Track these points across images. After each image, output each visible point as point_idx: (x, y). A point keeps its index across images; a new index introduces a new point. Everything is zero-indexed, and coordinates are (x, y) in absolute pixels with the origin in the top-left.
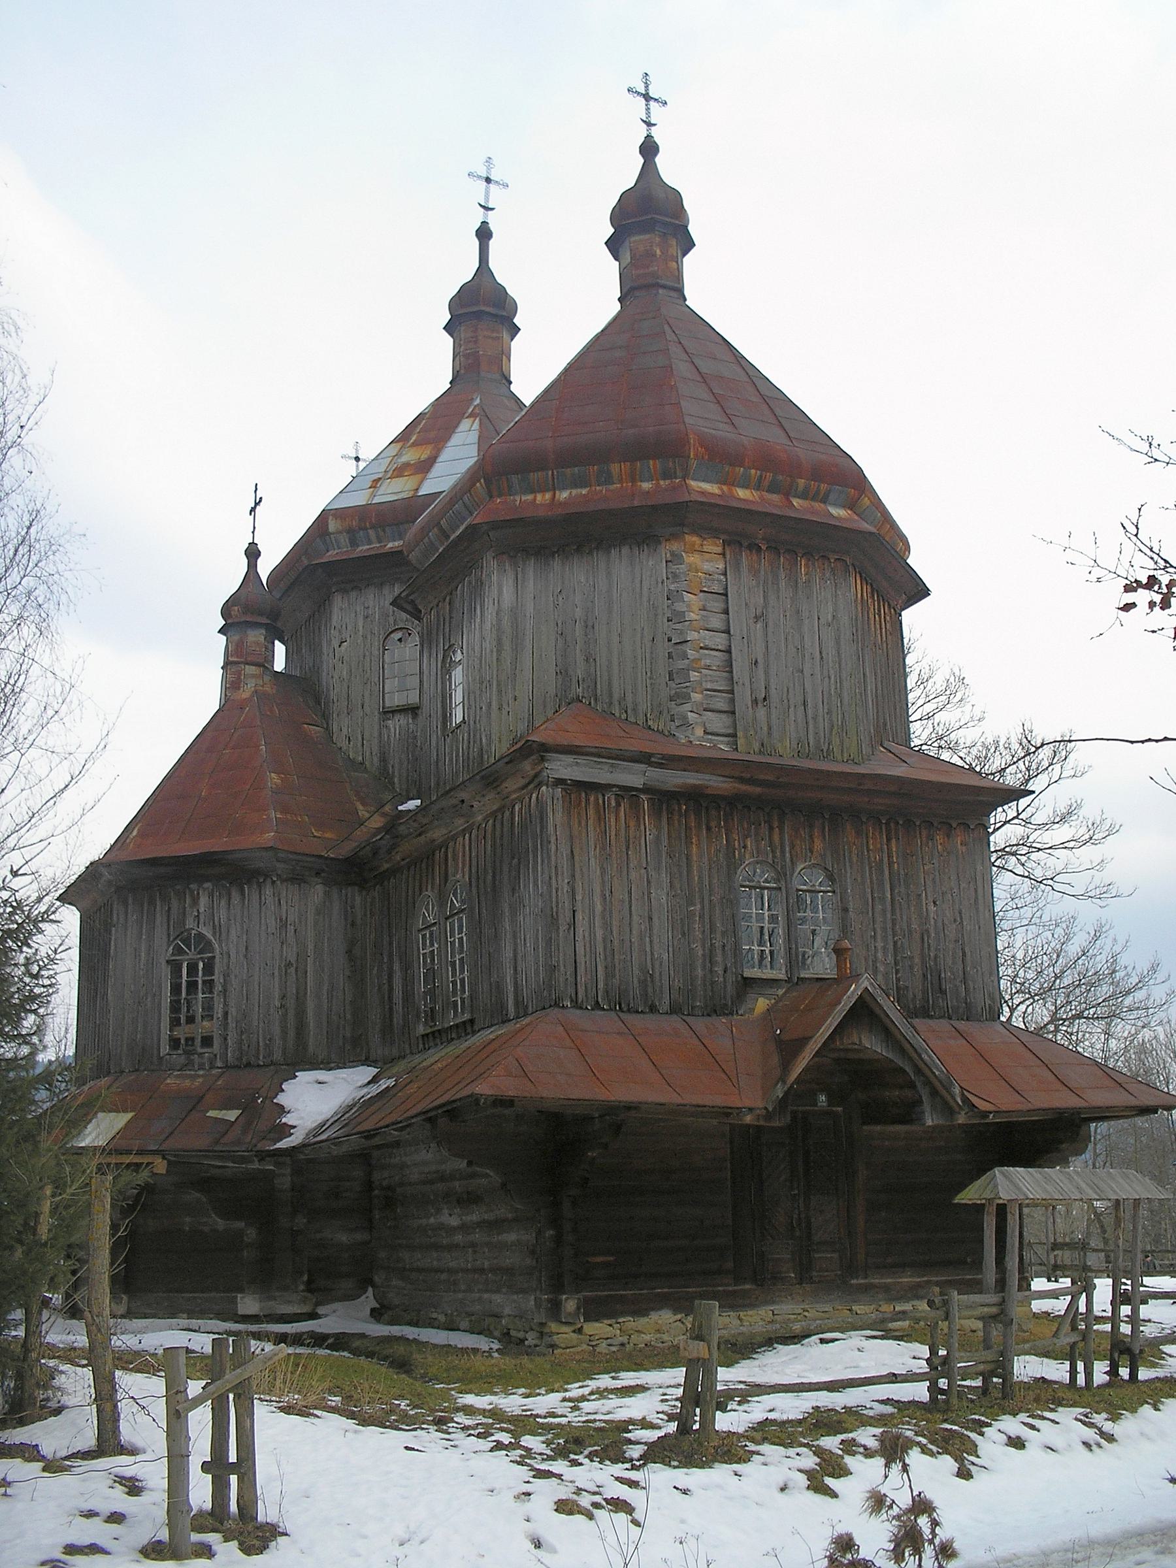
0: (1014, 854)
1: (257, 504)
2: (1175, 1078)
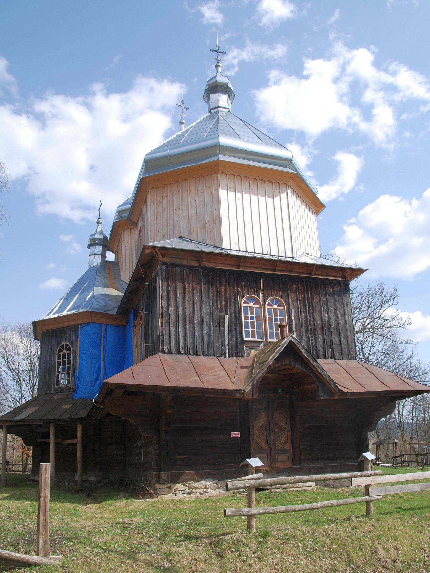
0: (377, 329)
1: (100, 206)
2: (429, 379)
